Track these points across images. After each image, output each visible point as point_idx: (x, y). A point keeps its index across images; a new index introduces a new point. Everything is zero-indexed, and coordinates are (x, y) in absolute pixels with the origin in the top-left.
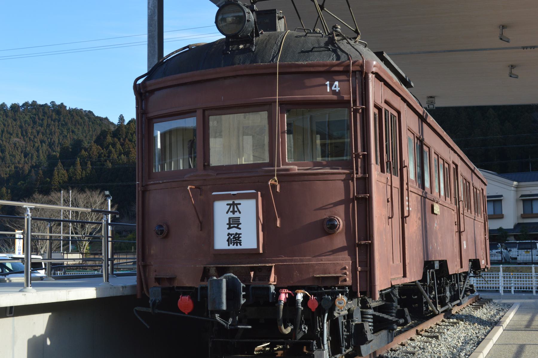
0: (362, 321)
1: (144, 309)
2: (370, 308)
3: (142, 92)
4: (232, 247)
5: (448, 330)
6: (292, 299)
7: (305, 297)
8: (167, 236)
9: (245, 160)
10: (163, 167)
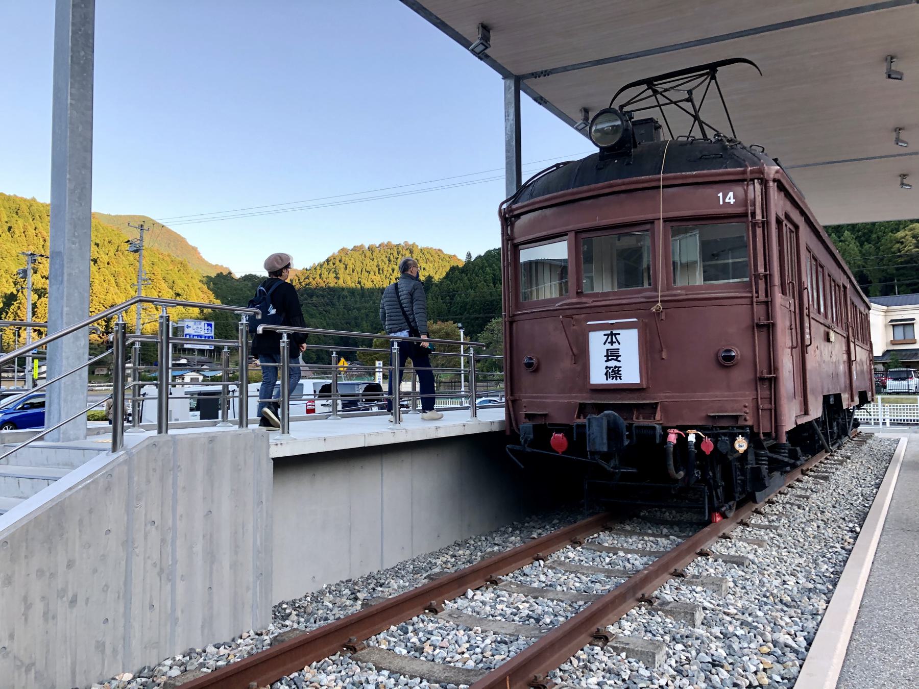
0: (757, 464)
1: (517, 447)
2: (763, 449)
3: (508, 218)
4: (610, 381)
5: (837, 469)
6: (682, 440)
7: (698, 437)
8: (536, 371)
9: (554, 296)
10: (538, 297)
